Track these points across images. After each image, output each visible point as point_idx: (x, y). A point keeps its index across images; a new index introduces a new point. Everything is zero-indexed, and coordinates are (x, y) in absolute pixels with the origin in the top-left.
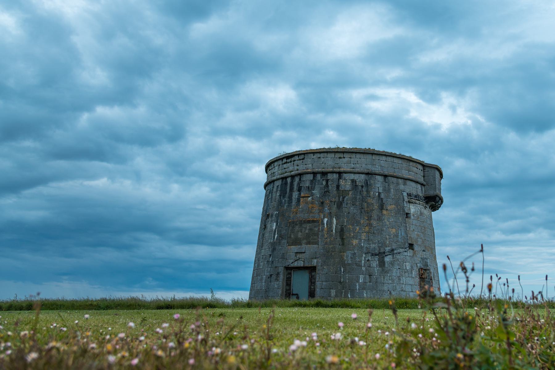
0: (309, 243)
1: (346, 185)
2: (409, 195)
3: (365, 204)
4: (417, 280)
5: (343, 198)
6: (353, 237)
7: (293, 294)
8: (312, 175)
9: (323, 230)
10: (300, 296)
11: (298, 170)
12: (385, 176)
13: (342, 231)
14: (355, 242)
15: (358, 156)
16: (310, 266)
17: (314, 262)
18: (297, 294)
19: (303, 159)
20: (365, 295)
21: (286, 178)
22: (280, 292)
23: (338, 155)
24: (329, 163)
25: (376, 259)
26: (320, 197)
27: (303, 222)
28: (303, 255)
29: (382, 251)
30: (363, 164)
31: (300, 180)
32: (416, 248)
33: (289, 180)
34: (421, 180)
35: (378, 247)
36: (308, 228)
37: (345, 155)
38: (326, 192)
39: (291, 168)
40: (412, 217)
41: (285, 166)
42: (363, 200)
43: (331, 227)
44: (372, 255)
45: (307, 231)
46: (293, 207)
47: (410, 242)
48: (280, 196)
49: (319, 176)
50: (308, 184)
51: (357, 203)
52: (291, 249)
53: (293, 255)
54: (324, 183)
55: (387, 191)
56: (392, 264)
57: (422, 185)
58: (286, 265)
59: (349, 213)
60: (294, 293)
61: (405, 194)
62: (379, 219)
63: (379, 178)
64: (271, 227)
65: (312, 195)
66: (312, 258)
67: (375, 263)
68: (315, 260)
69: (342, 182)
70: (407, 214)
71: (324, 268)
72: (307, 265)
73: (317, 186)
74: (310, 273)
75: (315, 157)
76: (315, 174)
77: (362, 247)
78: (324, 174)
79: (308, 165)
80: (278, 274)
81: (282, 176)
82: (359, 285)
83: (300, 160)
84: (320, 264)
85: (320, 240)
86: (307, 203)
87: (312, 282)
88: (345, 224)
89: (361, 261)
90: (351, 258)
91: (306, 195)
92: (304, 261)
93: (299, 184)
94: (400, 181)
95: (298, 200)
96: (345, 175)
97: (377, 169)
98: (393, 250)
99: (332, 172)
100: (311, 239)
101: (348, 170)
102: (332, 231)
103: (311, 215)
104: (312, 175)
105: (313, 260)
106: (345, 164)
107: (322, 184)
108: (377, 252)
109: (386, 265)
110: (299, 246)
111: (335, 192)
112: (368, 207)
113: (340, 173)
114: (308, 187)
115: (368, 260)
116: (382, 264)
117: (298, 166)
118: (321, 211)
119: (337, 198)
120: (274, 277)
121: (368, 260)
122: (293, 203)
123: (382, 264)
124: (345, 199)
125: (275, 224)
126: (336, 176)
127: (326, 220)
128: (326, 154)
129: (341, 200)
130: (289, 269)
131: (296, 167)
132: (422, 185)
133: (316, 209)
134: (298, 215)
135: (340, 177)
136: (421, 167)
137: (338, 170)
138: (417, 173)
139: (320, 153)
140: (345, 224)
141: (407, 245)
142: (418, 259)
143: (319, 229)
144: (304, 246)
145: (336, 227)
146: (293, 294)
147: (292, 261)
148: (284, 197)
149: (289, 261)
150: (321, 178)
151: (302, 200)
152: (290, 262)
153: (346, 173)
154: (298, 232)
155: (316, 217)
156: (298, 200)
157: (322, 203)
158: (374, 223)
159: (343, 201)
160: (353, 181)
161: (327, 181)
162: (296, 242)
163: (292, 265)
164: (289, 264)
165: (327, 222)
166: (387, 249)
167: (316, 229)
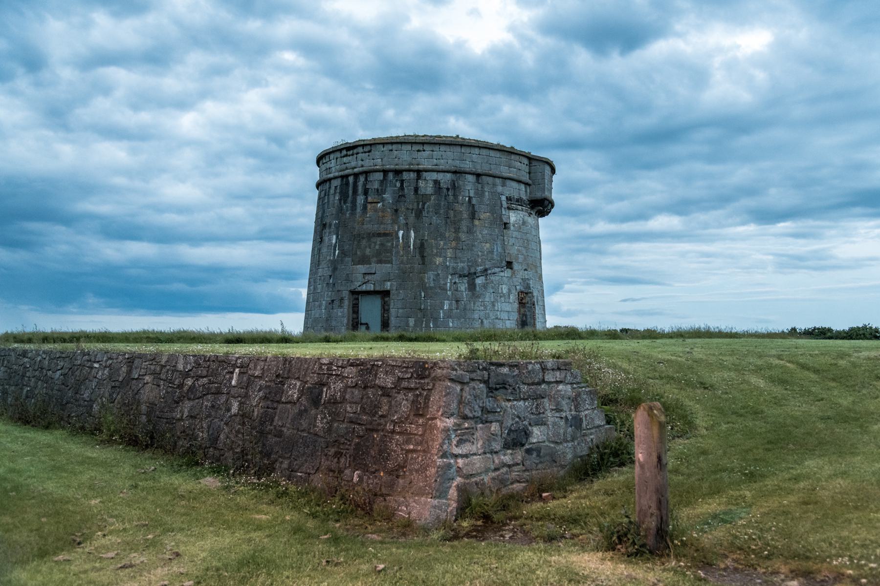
0: (380, 262)
1: (426, 187)
2: (509, 199)
3: (452, 213)
4: (516, 305)
5: (424, 204)
7: (361, 324)
8: (382, 174)
9: (397, 246)
10: (370, 325)
11: (362, 166)
12: (478, 175)
13: (421, 247)
14: (438, 260)
15: (443, 148)
17: (388, 286)
18: (367, 324)
19: (369, 152)
20: (451, 324)
21: (347, 176)
22: (345, 321)
23: (416, 147)
24: (404, 158)
25: (465, 281)
27: (371, 235)
29: (472, 271)
30: (448, 158)
31: (366, 179)
32: (516, 266)
34: (525, 178)
37: (426, 147)
38: (400, 196)
39: (353, 164)
40: (512, 228)
41: (345, 159)
45: (377, 247)
47: (508, 259)
48: (340, 200)
49: (391, 176)
50: (376, 185)
53: (360, 277)
54: (398, 184)
57: (526, 184)
58: (352, 288)
60: (363, 322)
61: (504, 198)
62: (470, 231)
63: (471, 178)
64: (330, 240)
65: (383, 200)
67: (463, 287)
68: (389, 283)
69: (421, 184)
70: (505, 224)
73: (388, 189)
74: (383, 299)
76: (385, 172)
77: (447, 267)
78: (398, 172)
80: (342, 299)
84: (394, 288)
86: (376, 210)
87: (385, 309)
89: (446, 284)
93: (365, 185)
94: (498, 181)
95: (365, 208)
96: (425, 174)
97: (467, 166)
98: (486, 270)
99: (409, 171)
103: (382, 226)
108: (466, 272)
109: (478, 289)
112: (455, 216)
113: (419, 172)
114: (378, 190)
115: (455, 283)
116: (472, 286)
118: (395, 221)
119: (415, 204)
120: (337, 303)
121: (455, 283)
123: (472, 286)
125: (334, 237)
126: (413, 175)
127: (401, 233)
131: (360, 163)
132: (526, 184)
133: (388, 219)
134: (365, 226)
135: (419, 177)
136: (526, 161)
137: (416, 167)
138: (521, 169)
139: (392, 143)
141: (504, 263)
142: (517, 280)
145: (414, 241)
146: (361, 324)
148: (345, 203)
151: (369, 206)
152: (356, 285)
156: (365, 208)
157: (396, 211)
158: (463, 236)
160: (436, 182)
161: (402, 182)
163: (359, 289)
165: (403, 235)
166: (479, 269)
167: (389, 244)
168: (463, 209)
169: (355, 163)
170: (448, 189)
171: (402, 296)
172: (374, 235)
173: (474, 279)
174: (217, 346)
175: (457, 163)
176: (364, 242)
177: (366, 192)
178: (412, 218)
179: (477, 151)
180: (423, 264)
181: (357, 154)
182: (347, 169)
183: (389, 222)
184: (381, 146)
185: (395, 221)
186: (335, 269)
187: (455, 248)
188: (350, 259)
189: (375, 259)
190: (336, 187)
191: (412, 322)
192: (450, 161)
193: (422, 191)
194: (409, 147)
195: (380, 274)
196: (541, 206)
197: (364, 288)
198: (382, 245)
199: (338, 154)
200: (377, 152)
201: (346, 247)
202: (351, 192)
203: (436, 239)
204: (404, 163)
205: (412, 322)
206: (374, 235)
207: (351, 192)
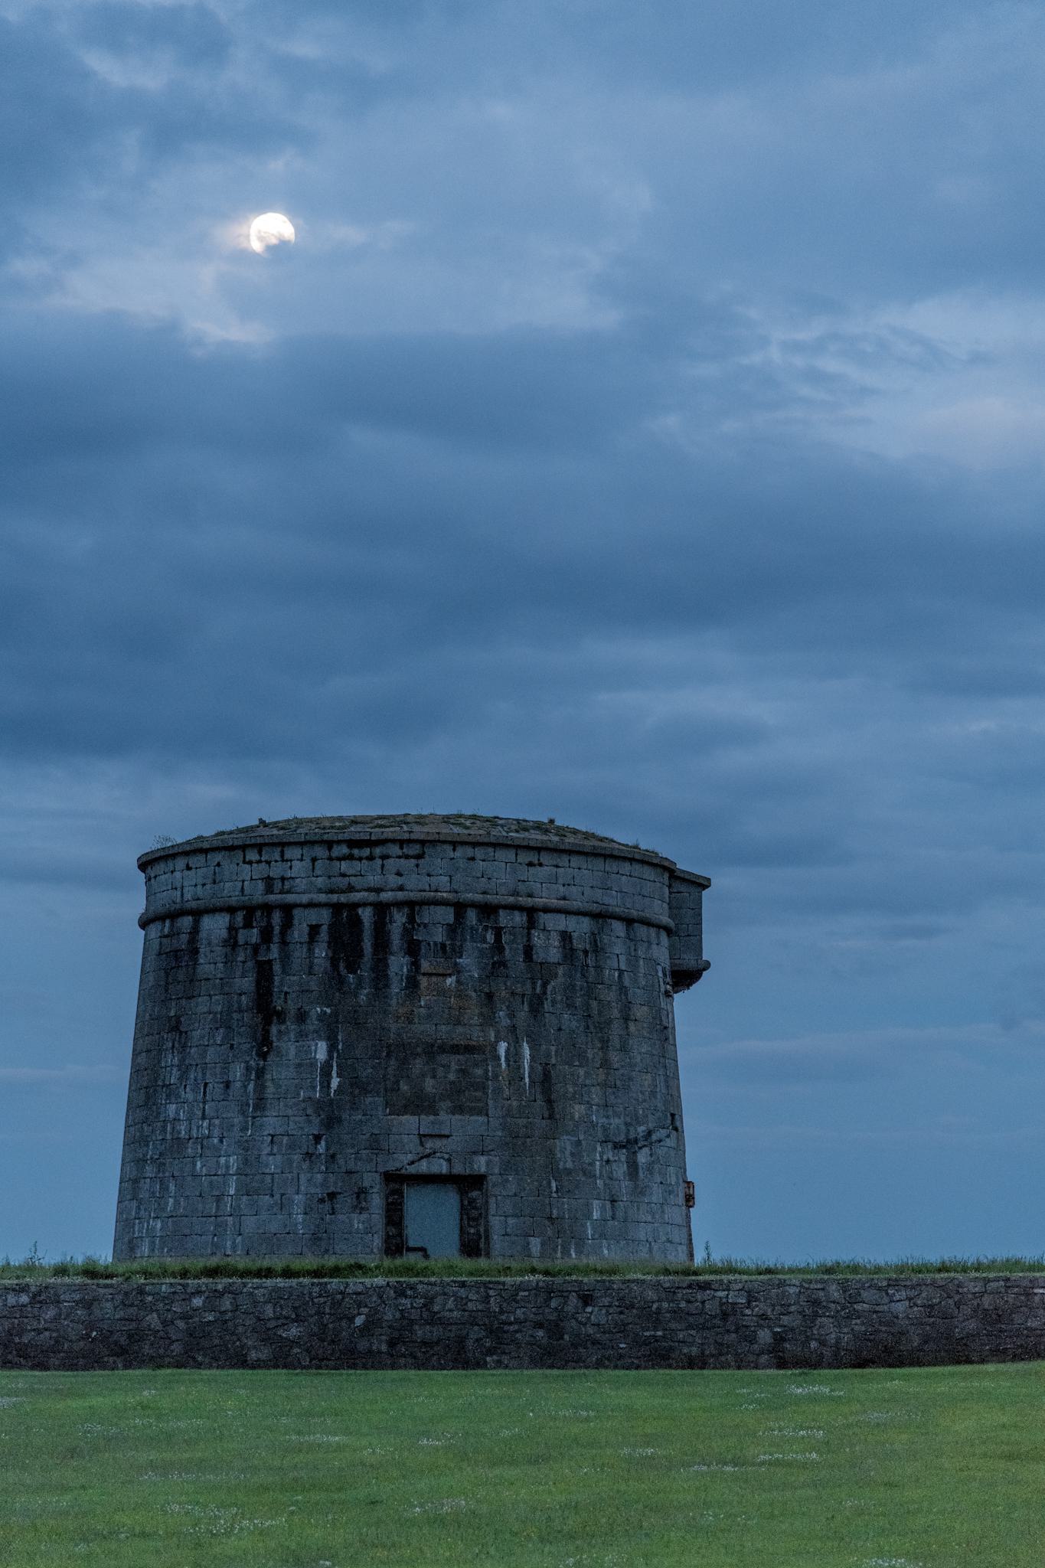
0: (459, 1109)
1: (548, 948)
3: (594, 1004)
5: (544, 985)
6: (573, 1098)
7: (410, 1249)
8: (451, 910)
9: (496, 1076)
11: (401, 888)
12: (629, 922)
13: (545, 1080)
14: (578, 1110)
15: (576, 861)
16: (468, 1172)
17: (481, 1164)
18: (423, 1250)
19: (419, 857)
23: (525, 857)
24: (499, 876)
25: (623, 1158)
26: (480, 979)
27: (433, 1050)
28: (445, 1141)
29: (632, 1136)
30: (582, 884)
31: (411, 919)
33: (399, 918)
34: (665, 919)
35: (626, 1124)
36: (454, 1067)
37: (545, 858)
38: (497, 966)
39: (374, 880)
41: (344, 866)
42: (590, 993)
43: (519, 1068)
44: (615, 1147)
45: (452, 1077)
46: (394, 1002)
48: (334, 962)
49: (472, 916)
50: (439, 936)
51: (578, 1001)
52: (401, 1123)
53: (411, 1143)
54: (490, 937)
55: (633, 961)
56: (650, 1169)
57: (669, 931)
58: (391, 1167)
59: (560, 1029)
60: (411, 1244)
62: (624, 1049)
63: (618, 927)
65: (458, 970)
66: (474, 1153)
67: (620, 1170)
68: (483, 1159)
69: (538, 938)
71: (507, 1181)
72: (458, 1169)
73: (468, 944)
74: (463, 1193)
75: (458, 854)
76: (460, 908)
77: (594, 1126)
78: (488, 910)
79: (437, 876)
80: (361, 1193)
81: (334, 898)
82: (593, 1228)
83: (407, 857)
84: (496, 1171)
85: (490, 1102)
86: (443, 992)
88: (553, 1061)
89: (592, 1164)
90: (572, 1154)
91: (441, 971)
92: (449, 1160)
93: (407, 933)
95: (412, 984)
96: (544, 918)
97: (613, 902)
98: (649, 1133)
100: (465, 1097)
101: (554, 903)
102: (522, 1079)
103: (460, 1029)
104: (451, 910)
105: (475, 1158)
106: (545, 884)
107: (484, 941)
108: (622, 1138)
110: (432, 1118)
111: (522, 966)
112: (600, 1013)
113: (531, 912)
114: (443, 946)
115: (608, 1161)
116: (633, 1167)
117: (399, 874)
118: (489, 1020)
119: (529, 985)
120: (345, 1202)
121: (608, 1161)
122: (395, 989)
123: (633, 1167)
124: (550, 988)
126: (519, 918)
127: (502, 1047)
128: (491, 850)
129: (538, 990)
130: (397, 1181)
131: (393, 880)
132: (669, 931)
133: (473, 1014)
134: (417, 1028)
135: (532, 924)
137: (529, 902)
140: (553, 1061)
143: (487, 1071)
144: (443, 1116)
145: (531, 1067)
147: (410, 1157)
148: (352, 968)
149: (402, 1157)
150: (480, 921)
151: (424, 982)
152: (401, 1161)
153: (547, 910)
154: (423, 1076)
155: (476, 1036)
156: (412, 984)
157: (490, 996)
158: (615, 1057)
159: (545, 993)
161: (498, 932)
162: (420, 1104)
163: (412, 1170)
164: (398, 1165)
165: (507, 1051)
167: (479, 1072)
168: (611, 996)
169: (371, 878)
170: (586, 952)
171: (512, 1188)
172: (443, 1049)
173: (635, 1153)
174: (279, 1280)
175: (598, 894)
176: (418, 1065)
177: (413, 949)
178: (523, 1013)
179: (626, 867)
180: (551, 1117)
181: (384, 857)
182: (351, 889)
183: (476, 1020)
184: (448, 848)
185: (489, 1020)
186: (331, 1122)
187: (604, 1085)
188: (380, 1100)
189: (446, 1104)
190: (314, 930)
191: (535, 1244)
192: (588, 891)
193: (539, 956)
194: (510, 855)
195: (460, 1137)
196: (685, 977)
197: (423, 1167)
198: (463, 1072)
199: (320, 851)
200: (438, 862)
201: (366, 1072)
202: (367, 945)
203: (571, 1065)
204: (503, 890)
205: (535, 1244)
206: (443, 1049)
207: (367, 945)
